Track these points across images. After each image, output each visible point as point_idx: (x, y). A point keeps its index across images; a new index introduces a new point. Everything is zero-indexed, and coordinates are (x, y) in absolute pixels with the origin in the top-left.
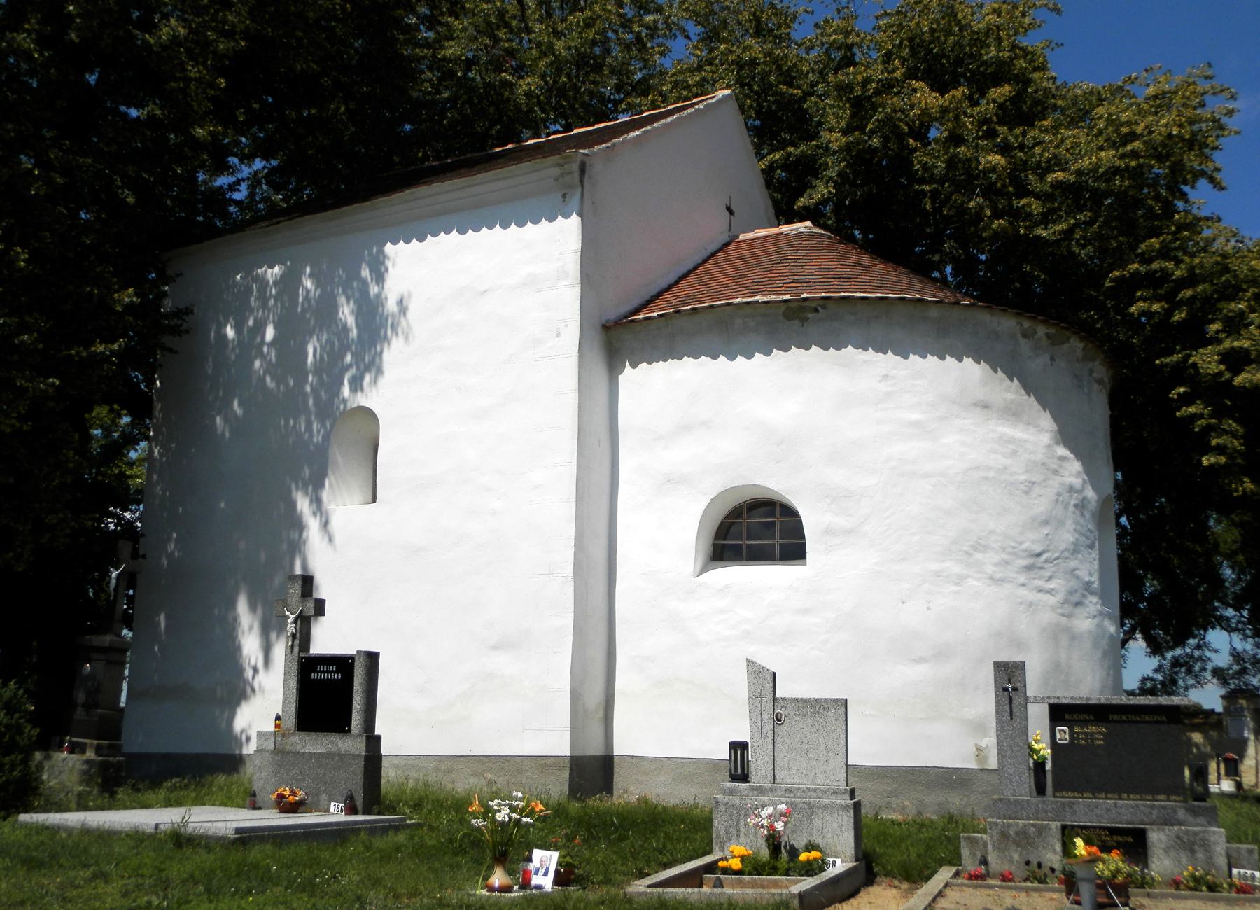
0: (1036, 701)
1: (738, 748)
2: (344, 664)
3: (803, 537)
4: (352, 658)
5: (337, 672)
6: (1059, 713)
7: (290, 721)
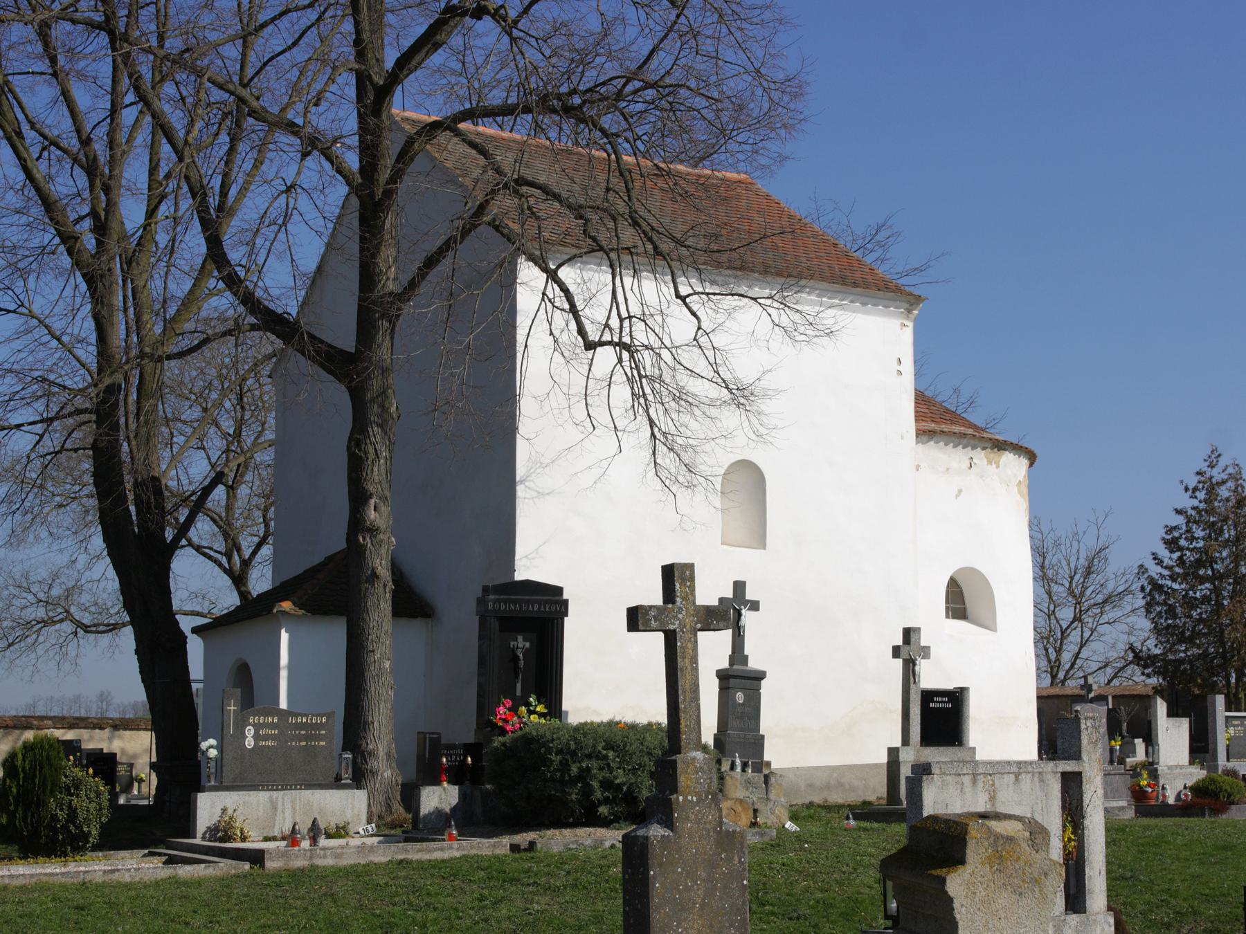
2: (957, 698)
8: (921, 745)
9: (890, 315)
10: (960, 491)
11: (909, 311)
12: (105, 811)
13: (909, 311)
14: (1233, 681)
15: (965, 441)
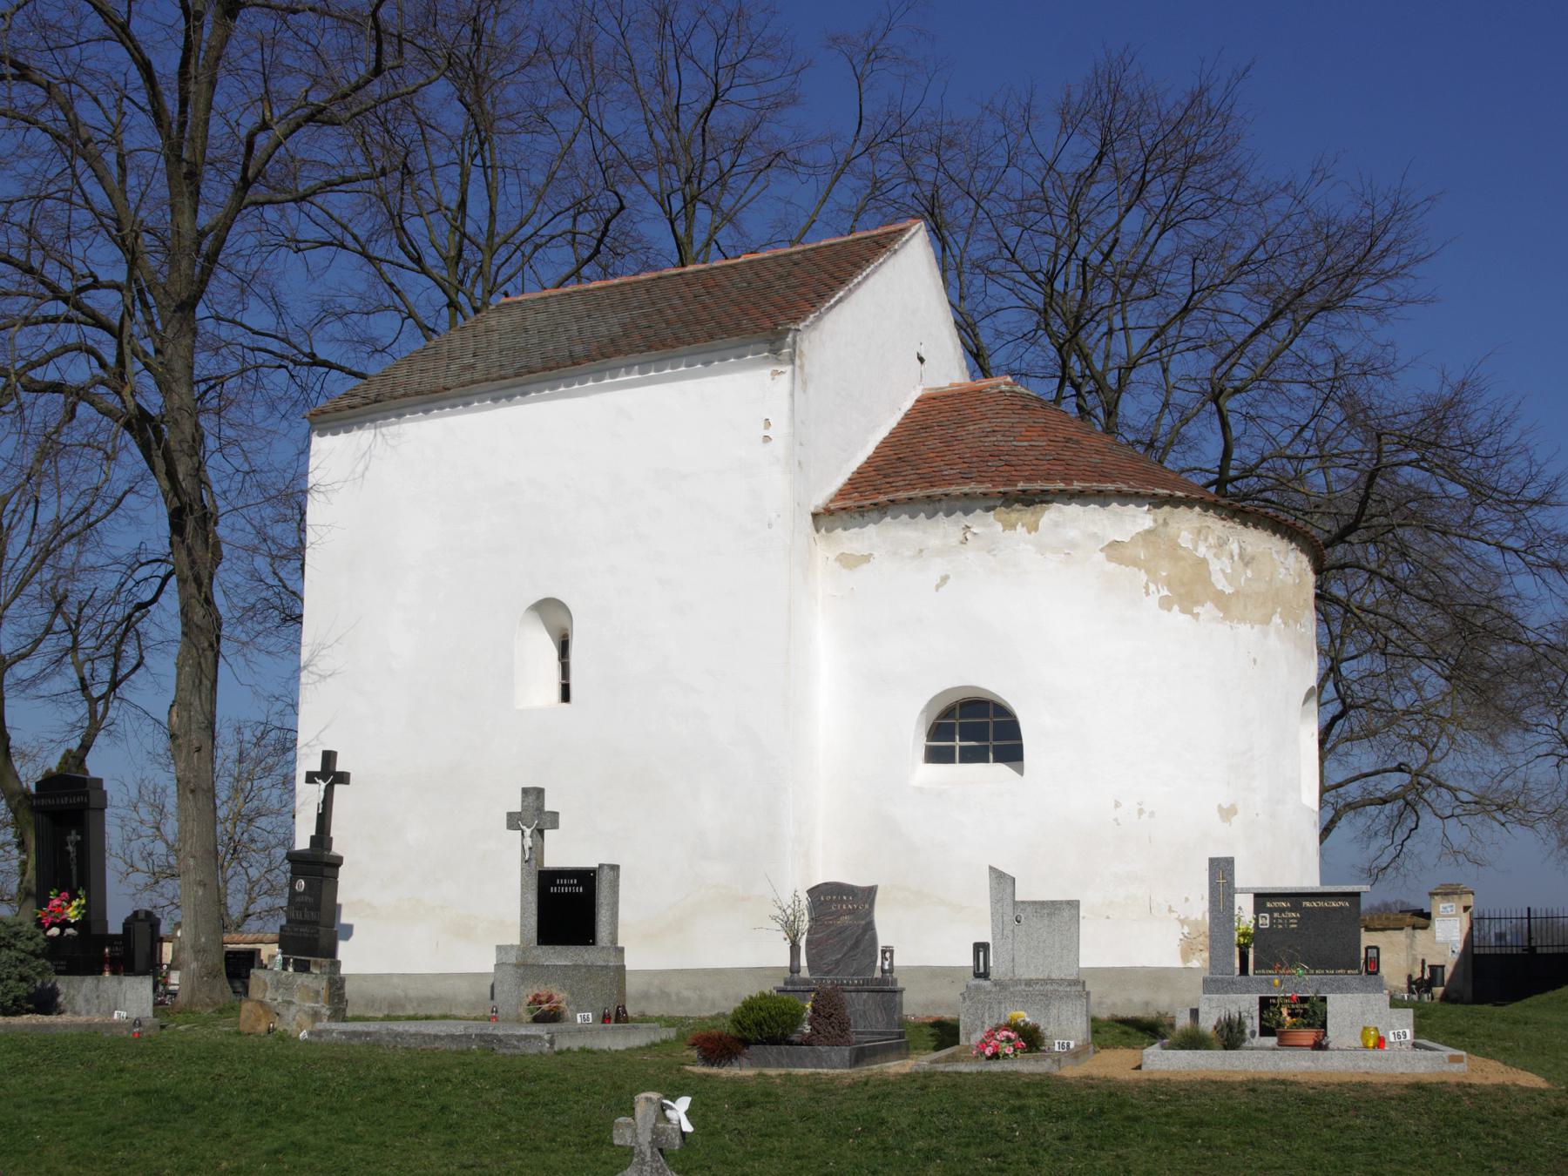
0: (1244, 891)
1: (980, 948)
2: (587, 878)
3: (1019, 737)
4: (594, 871)
5: (578, 885)
6: (1262, 899)
7: (533, 934)
8: (539, 944)
10: (945, 579)
11: (775, 352)
15: (944, 505)
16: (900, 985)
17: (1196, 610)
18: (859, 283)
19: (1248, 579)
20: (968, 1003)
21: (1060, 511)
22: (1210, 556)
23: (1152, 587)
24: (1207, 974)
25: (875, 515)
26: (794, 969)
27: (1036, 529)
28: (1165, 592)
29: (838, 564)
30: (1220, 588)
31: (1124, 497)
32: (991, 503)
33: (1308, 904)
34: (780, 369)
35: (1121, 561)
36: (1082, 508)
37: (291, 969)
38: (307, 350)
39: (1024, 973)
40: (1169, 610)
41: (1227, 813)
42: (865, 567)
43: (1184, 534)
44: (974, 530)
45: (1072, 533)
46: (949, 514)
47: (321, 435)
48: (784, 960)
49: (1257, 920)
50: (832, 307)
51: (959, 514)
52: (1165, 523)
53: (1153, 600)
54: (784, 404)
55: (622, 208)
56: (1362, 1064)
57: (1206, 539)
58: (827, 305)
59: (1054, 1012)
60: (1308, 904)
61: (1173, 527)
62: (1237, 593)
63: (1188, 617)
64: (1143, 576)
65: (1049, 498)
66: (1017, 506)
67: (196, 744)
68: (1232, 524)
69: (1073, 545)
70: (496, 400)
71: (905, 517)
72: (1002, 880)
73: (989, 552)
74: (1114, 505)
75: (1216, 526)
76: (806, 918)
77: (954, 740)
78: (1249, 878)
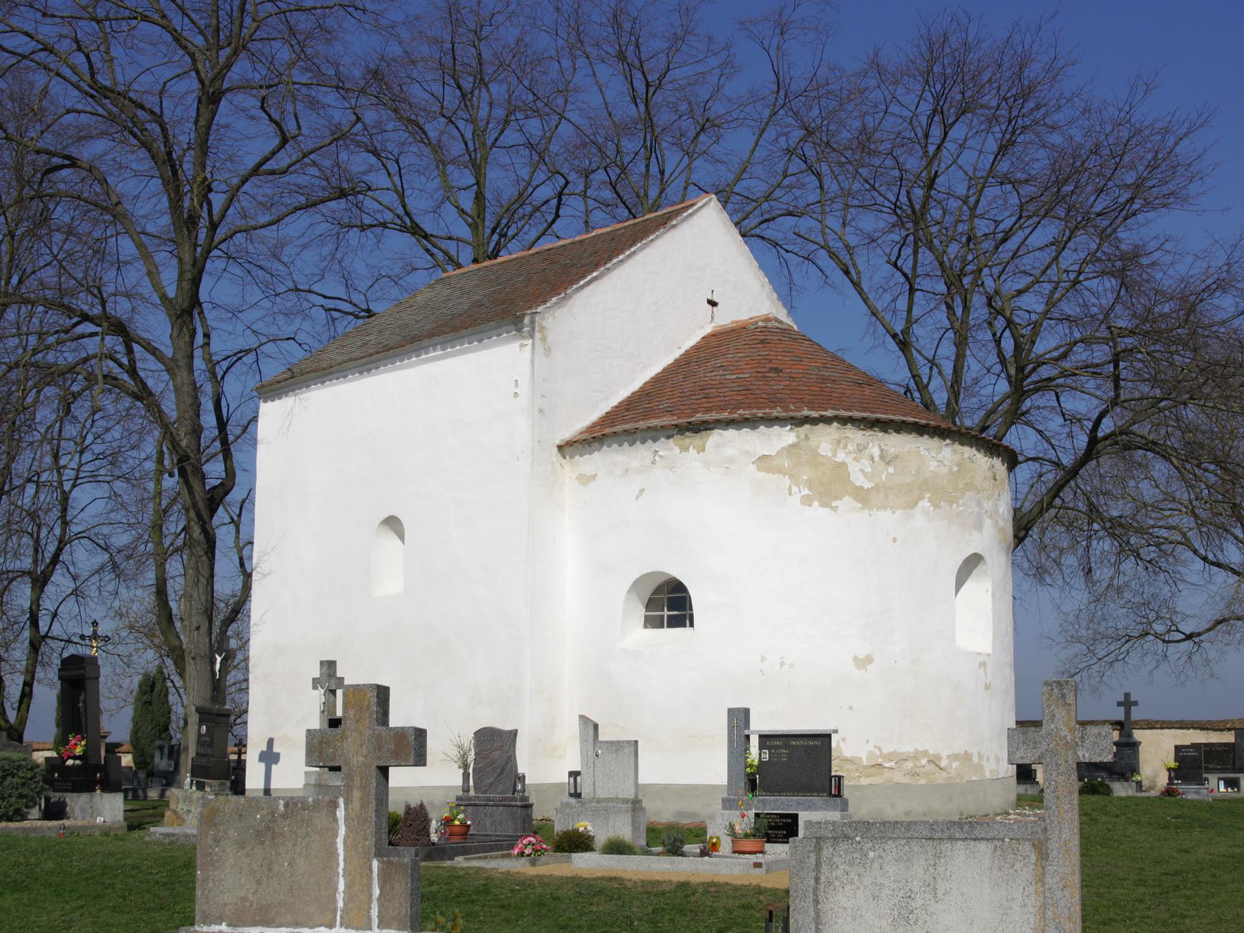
6: (765, 739)
9: (508, 341)
10: (642, 491)
11: (519, 330)
12: (520, 845)
13: (519, 330)
14: (218, 666)
15: (638, 436)
16: (531, 802)
17: (834, 504)
18: (621, 261)
19: (889, 475)
20: (559, 815)
21: (720, 435)
22: (849, 460)
23: (795, 489)
24: (725, 795)
25: (597, 445)
26: (466, 789)
27: (703, 450)
28: (806, 492)
29: (577, 482)
30: (858, 484)
31: (770, 421)
32: (670, 433)
33: (794, 743)
34: (525, 342)
35: (769, 470)
36: (737, 432)
37: (194, 788)
38: (364, 307)
39: (601, 794)
40: (810, 505)
41: (863, 662)
42: (593, 484)
43: (824, 445)
44: (661, 453)
45: (730, 452)
46: (643, 442)
47: (265, 402)
48: (459, 781)
49: (760, 755)
50: (583, 287)
51: (650, 441)
52: (807, 438)
53: (796, 499)
54: (527, 368)
55: (567, 183)
56: (700, 867)
57: (845, 447)
58: (575, 287)
59: (611, 822)
60: (794, 743)
61: (814, 440)
62: (877, 487)
63: (827, 510)
64: (787, 481)
65: (711, 426)
66: (687, 434)
67: (195, 625)
68: (872, 433)
69: (731, 460)
70: (361, 373)
71: (615, 446)
72: (590, 727)
73: (670, 469)
74: (762, 428)
75: (855, 435)
76: (473, 753)
77: (663, 611)
78: (760, 724)
